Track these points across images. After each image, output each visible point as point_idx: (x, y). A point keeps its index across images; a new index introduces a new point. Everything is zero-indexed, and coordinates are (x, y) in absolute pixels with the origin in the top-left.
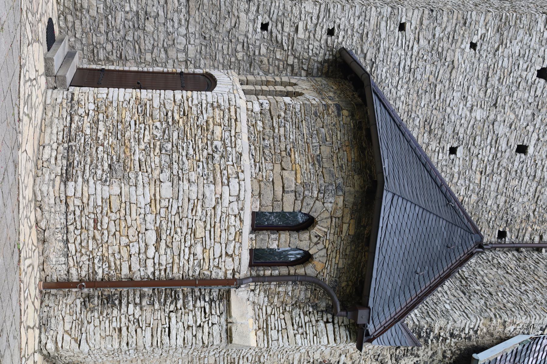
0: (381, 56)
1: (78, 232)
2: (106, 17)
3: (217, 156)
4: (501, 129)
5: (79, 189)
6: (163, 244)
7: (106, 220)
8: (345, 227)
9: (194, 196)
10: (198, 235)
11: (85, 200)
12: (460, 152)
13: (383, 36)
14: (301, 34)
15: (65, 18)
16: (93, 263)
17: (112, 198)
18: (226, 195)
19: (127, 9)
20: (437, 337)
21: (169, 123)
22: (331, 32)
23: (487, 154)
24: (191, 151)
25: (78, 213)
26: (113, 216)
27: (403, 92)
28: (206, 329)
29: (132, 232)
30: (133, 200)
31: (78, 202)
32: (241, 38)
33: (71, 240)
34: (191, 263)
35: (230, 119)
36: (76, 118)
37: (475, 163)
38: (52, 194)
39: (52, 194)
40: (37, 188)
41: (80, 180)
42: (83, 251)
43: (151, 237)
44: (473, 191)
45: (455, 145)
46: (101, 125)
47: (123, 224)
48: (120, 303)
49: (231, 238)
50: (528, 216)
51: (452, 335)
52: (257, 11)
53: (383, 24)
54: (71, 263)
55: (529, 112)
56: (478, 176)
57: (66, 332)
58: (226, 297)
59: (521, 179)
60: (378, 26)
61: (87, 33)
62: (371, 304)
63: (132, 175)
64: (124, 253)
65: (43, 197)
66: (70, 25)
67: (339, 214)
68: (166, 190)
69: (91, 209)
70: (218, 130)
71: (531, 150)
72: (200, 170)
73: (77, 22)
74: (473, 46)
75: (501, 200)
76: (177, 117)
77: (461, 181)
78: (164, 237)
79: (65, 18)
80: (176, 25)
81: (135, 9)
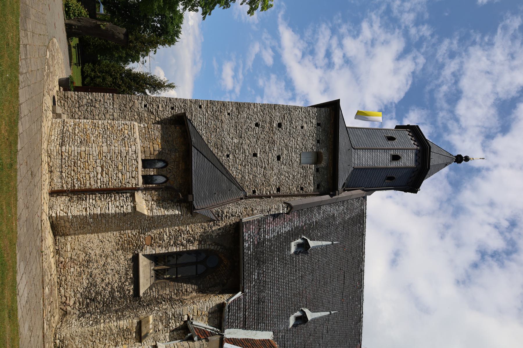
0: (193, 117)
1: (66, 168)
2: (79, 102)
3: (126, 139)
4: (245, 147)
5: (67, 148)
6: (104, 173)
7: (79, 162)
8: (180, 165)
9: (117, 151)
10: (120, 168)
11: (70, 153)
12: (231, 156)
13: (193, 110)
14: (160, 108)
15: (60, 102)
16: (74, 182)
17: (82, 152)
18: (130, 151)
19: (88, 98)
20: (226, 216)
21: (105, 129)
22: (172, 108)
23: (242, 157)
24: (115, 137)
25: (67, 159)
26: (82, 160)
27: (204, 132)
28: (125, 207)
29: (90, 167)
30: (91, 153)
31: (67, 154)
32: (136, 110)
33: (64, 171)
34: (117, 181)
35: (131, 128)
36: (66, 127)
37: (238, 161)
38: (55, 150)
39: (55, 150)
40: (49, 148)
41: (68, 146)
42: (69, 176)
43: (99, 169)
44: (239, 173)
45: (229, 153)
46: (76, 129)
47: (87, 164)
48: (86, 199)
49: (134, 170)
50: (263, 184)
51: (232, 215)
52: (142, 100)
53: (193, 105)
54: (64, 182)
55: (255, 140)
56: (240, 166)
57: (61, 210)
58: (133, 196)
59: (257, 167)
60: (191, 106)
61: (70, 108)
62: (194, 193)
63: (90, 145)
64: (87, 176)
65: (51, 152)
66: (63, 104)
67: (177, 160)
68: (105, 149)
69: (72, 157)
70: (126, 132)
71: (258, 155)
72: (119, 143)
73: (66, 103)
74: (229, 114)
75: (251, 177)
76: (109, 127)
77: (233, 169)
78: (105, 169)
79: (60, 102)
80: (109, 105)
81: (91, 98)
